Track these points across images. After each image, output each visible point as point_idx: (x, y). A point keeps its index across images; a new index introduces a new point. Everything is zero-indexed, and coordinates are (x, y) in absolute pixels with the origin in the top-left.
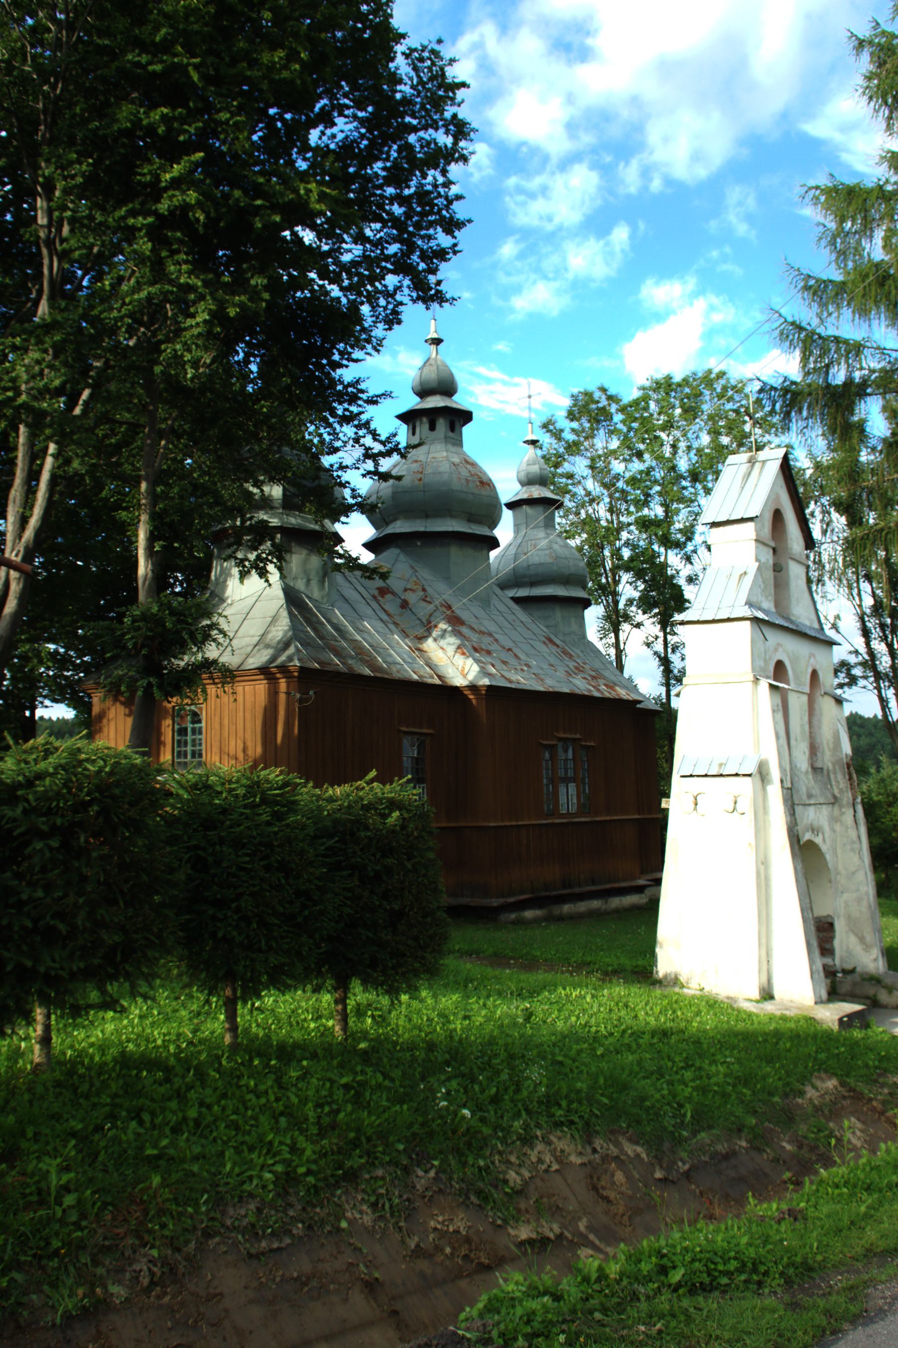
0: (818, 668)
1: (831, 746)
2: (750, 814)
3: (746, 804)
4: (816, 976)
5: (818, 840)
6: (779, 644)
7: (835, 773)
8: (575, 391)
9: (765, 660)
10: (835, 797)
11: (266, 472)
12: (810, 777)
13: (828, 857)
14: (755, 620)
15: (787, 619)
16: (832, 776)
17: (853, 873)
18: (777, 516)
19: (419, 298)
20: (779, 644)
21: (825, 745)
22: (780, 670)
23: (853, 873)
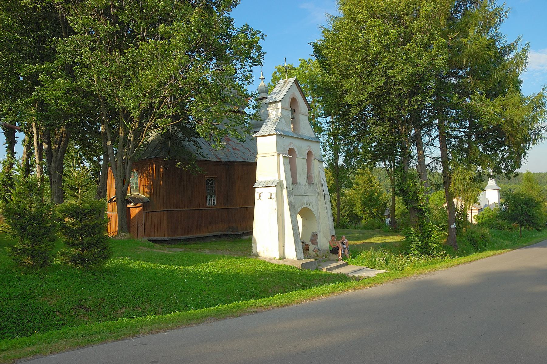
0: (311, 150)
1: (317, 176)
2: (275, 199)
3: (274, 196)
4: (298, 251)
5: (310, 207)
6: (291, 143)
7: (319, 185)
8: (277, 66)
9: (284, 148)
10: (318, 193)
11: (441, 140)
12: (307, 186)
13: (315, 213)
14: (277, 134)
15: (298, 135)
16: (318, 186)
17: (325, 218)
18: (293, 101)
19: (254, 34)
20: (291, 143)
21: (316, 176)
22: (291, 151)
23: (325, 218)
